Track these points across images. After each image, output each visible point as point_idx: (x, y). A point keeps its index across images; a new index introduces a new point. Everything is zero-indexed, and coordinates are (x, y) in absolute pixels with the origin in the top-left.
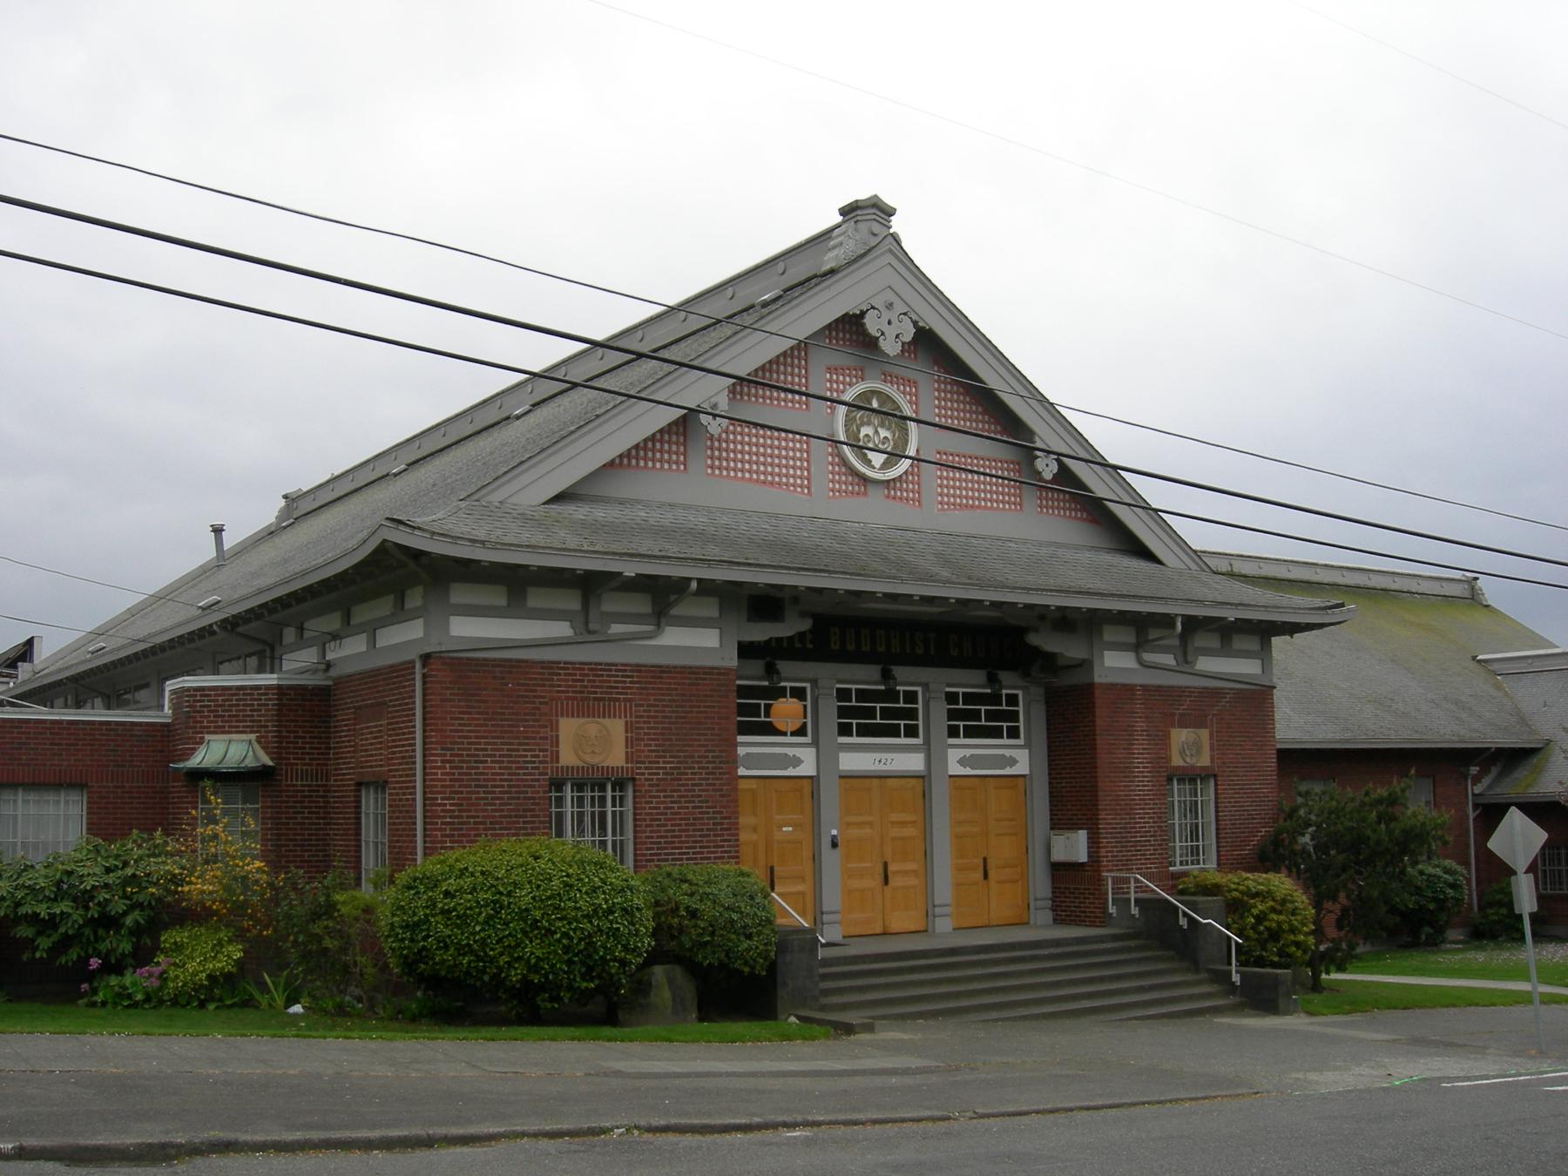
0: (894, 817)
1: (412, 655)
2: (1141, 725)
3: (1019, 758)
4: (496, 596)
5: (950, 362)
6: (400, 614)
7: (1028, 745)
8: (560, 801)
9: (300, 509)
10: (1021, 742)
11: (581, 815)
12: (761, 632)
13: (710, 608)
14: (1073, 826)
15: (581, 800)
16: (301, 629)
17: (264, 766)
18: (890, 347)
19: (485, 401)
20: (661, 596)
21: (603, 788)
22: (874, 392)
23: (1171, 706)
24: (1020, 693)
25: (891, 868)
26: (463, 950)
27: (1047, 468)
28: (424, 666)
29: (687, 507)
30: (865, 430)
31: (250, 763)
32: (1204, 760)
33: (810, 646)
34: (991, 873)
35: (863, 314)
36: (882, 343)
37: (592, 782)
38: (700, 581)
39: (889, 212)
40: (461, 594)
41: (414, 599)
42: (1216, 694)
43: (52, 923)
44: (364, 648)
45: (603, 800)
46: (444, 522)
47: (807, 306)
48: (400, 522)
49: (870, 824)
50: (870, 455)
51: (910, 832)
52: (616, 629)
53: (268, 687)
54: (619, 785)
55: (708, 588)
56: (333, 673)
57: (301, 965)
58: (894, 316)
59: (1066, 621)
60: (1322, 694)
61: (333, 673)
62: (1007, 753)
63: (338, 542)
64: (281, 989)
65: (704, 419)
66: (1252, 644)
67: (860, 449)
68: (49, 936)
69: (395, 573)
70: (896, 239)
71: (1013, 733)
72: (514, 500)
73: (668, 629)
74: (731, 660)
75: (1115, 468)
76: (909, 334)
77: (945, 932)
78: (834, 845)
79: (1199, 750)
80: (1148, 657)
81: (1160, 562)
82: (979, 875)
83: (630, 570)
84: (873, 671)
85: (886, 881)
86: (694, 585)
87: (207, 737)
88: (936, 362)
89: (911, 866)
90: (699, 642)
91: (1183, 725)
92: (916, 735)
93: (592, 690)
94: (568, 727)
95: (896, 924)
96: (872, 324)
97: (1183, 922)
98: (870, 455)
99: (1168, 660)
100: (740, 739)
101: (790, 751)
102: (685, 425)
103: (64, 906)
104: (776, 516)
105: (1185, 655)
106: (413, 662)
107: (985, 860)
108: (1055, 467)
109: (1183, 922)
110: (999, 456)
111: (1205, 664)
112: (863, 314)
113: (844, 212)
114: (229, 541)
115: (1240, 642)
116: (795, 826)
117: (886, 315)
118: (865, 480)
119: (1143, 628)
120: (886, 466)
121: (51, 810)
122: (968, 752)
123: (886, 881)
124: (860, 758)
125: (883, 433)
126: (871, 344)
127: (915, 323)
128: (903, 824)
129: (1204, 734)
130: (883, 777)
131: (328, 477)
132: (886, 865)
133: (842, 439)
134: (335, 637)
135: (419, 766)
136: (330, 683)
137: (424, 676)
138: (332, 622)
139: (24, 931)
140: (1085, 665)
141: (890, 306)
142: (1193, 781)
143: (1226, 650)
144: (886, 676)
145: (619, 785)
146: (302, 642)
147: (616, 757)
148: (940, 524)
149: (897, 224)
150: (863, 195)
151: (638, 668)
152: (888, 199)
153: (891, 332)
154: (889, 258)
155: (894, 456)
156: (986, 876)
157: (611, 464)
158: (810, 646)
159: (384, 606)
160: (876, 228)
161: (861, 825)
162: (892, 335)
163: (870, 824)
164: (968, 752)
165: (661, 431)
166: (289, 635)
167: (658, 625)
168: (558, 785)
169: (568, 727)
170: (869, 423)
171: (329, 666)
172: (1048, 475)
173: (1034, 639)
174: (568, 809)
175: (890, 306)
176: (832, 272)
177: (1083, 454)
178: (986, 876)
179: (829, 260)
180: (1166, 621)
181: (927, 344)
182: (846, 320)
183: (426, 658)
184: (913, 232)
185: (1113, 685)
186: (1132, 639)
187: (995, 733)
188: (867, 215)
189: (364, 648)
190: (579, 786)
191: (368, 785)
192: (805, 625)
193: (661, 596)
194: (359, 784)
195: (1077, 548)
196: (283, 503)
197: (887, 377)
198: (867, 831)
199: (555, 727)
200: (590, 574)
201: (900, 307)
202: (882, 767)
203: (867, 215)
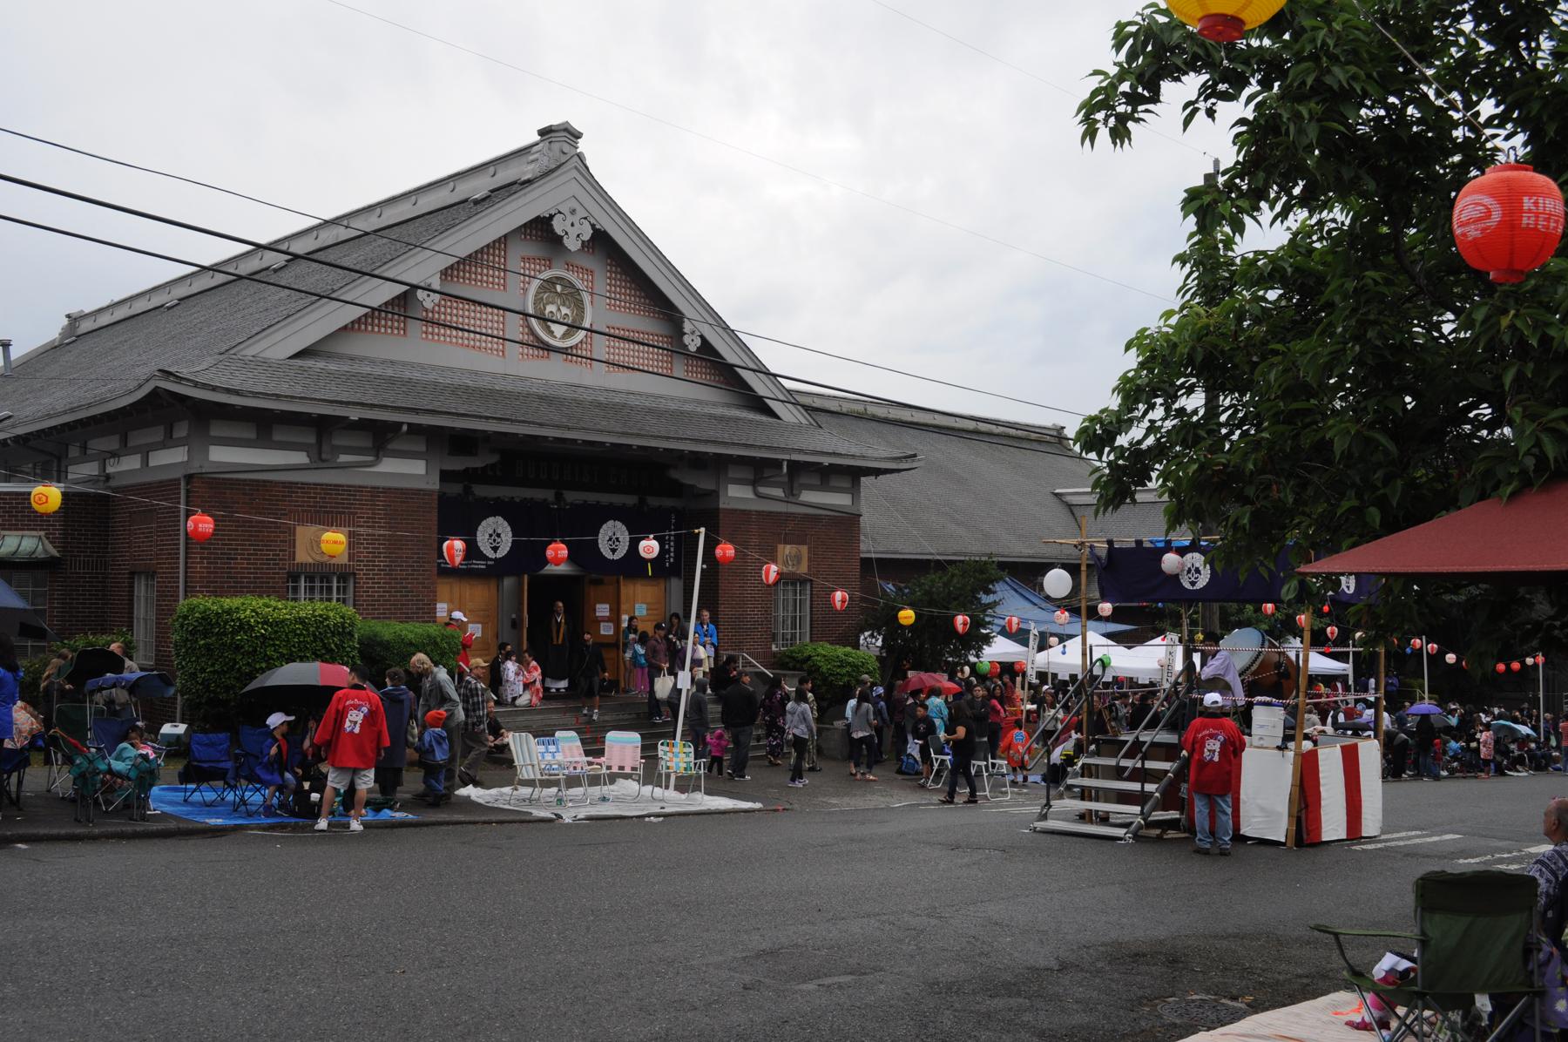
1: (178, 474)
5: (619, 258)
6: (168, 442)
9: (80, 332)
12: (457, 464)
16: (84, 448)
17: (53, 557)
18: (572, 244)
20: (381, 436)
27: (693, 344)
29: (404, 364)
30: (550, 308)
31: (40, 554)
32: (803, 569)
35: (551, 217)
36: (566, 241)
38: (409, 425)
39: (578, 136)
40: (217, 430)
41: (181, 431)
42: (816, 518)
44: (138, 466)
45: (330, 589)
46: (202, 368)
47: (508, 209)
48: (170, 373)
50: (554, 327)
52: (343, 458)
55: (415, 429)
56: (113, 483)
58: (576, 219)
59: (698, 461)
60: (891, 522)
61: (113, 483)
63: (121, 380)
65: (420, 294)
66: (845, 483)
67: (544, 320)
69: (166, 411)
70: (580, 157)
72: (267, 354)
73: (385, 460)
74: (434, 484)
75: (775, 376)
76: (587, 234)
79: (799, 562)
80: (762, 490)
81: (771, 413)
83: (354, 415)
86: (405, 428)
88: (609, 256)
90: (408, 470)
94: (304, 533)
96: (558, 226)
99: (778, 492)
102: (404, 304)
104: (476, 373)
105: (791, 491)
108: (698, 342)
110: (649, 329)
112: (551, 217)
113: (542, 133)
114: (16, 353)
115: (835, 482)
117: (570, 219)
118: (548, 348)
119: (759, 469)
120: (565, 336)
125: (564, 310)
126: (555, 241)
127: (593, 226)
129: (804, 549)
133: (531, 311)
134: (114, 455)
135: (182, 561)
137: (188, 491)
138: (112, 443)
140: (714, 494)
141: (573, 212)
142: (794, 584)
143: (824, 486)
146: (85, 457)
148: (597, 376)
149: (583, 146)
150: (555, 121)
152: (577, 125)
153: (573, 232)
154: (575, 174)
155: (573, 327)
157: (345, 328)
159: (157, 434)
160: (566, 148)
162: (574, 234)
165: (386, 304)
166: (74, 452)
168: (294, 577)
169: (304, 533)
171: (108, 477)
172: (693, 348)
173: (675, 474)
175: (573, 212)
176: (529, 182)
177: (752, 366)
179: (525, 170)
180: (777, 464)
181: (601, 242)
182: (543, 223)
183: (189, 478)
184: (601, 156)
185: (734, 511)
186: (751, 477)
188: (560, 136)
189: (138, 466)
190: (310, 578)
191: (140, 573)
192: (493, 459)
193: (381, 436)
194: (132, 574)
195: (715, 404)
197: (569, 266)
200: (322, 417)
201: (581, 213)
203: (560, 136)
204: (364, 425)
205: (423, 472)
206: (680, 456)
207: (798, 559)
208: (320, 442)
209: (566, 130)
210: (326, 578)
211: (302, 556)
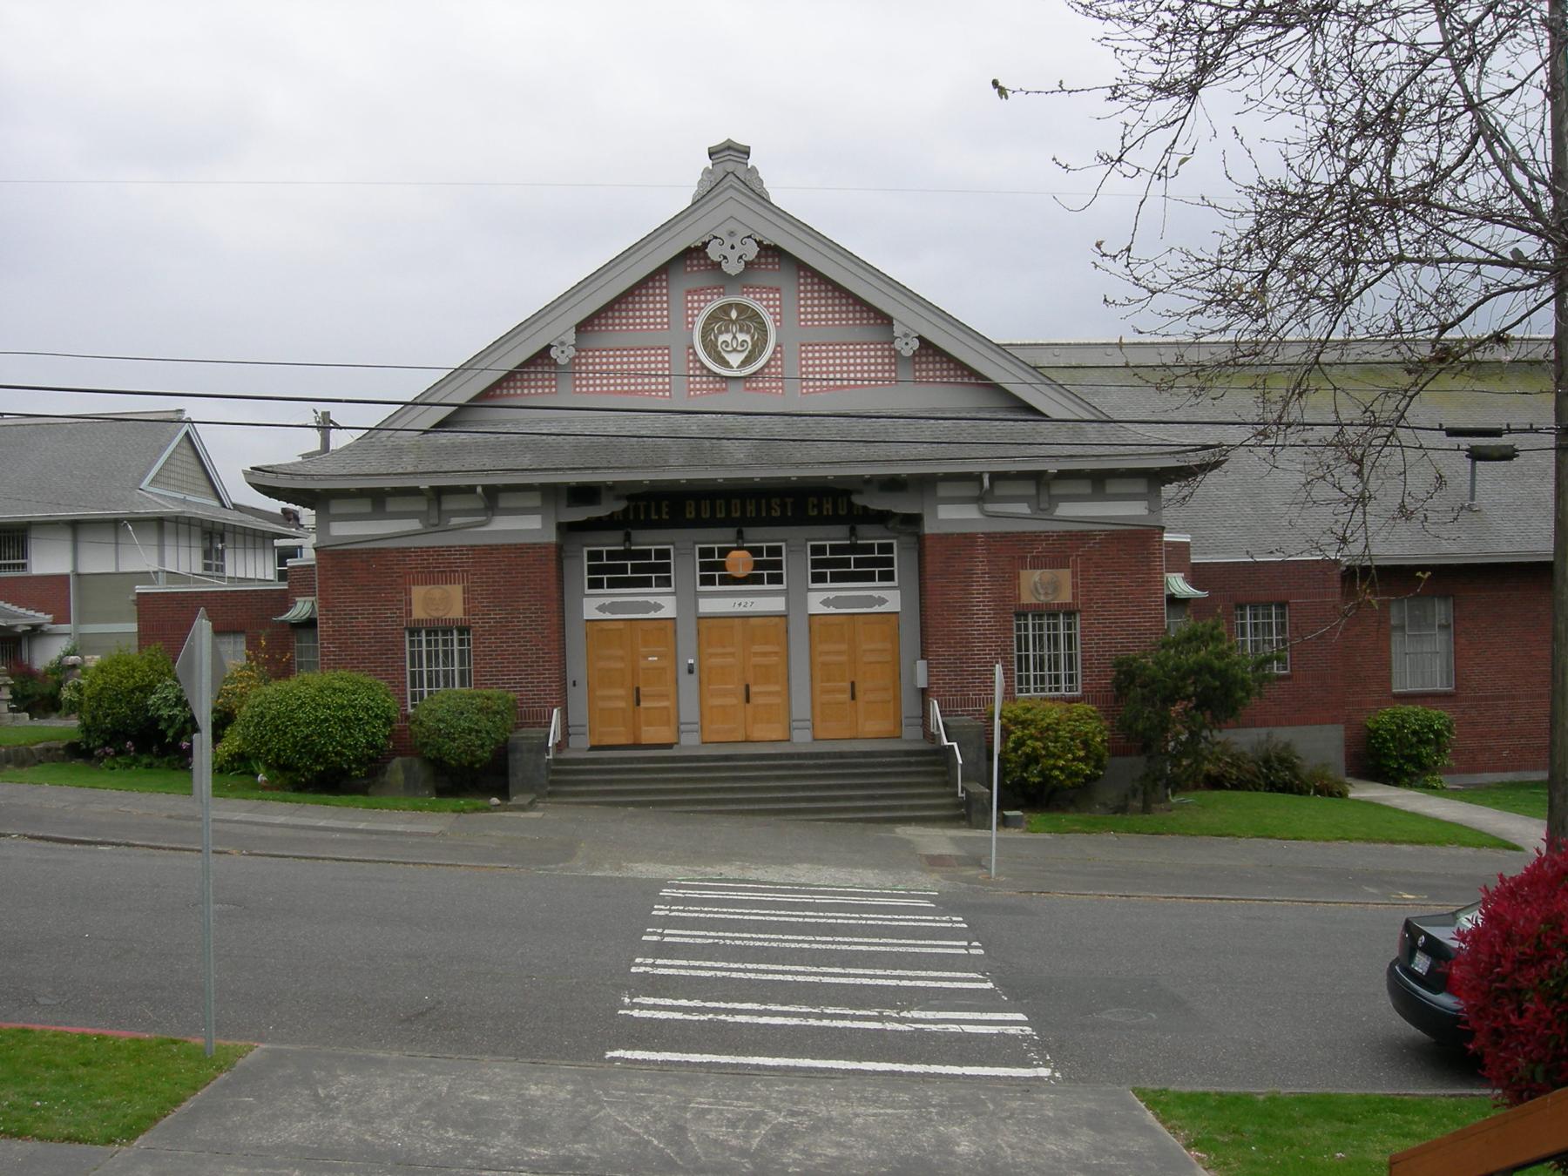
0: (757, 648)
2: (980, 568)
3: (890, 598)
8: (1243, 617)
10: (895, 583)
11: (1041, 636)
13: (535, 500)
18: (733, 267)
20: (493, 498)
21: (1026, 616)
22: (730, 305)
23: (1016, 550)
24: (895, 542)
25: (753, 689)
27: (908, 347)
33: (665, 517)
34: (858, 694)
37: (439, 629)
39: (746, 152)
42: (1083, 536)
49: (732, 654)
51: (844, 658)
52: (455, 521)
54: (1070, 614)
59: (893, 484)
62: (876, 594)
71: (888, 576)
74: (551, 537)
77: (802, 740)
78: (691, 671)
80: (992, 508)
82: (846, 696)
84: (843, 530)
85: (748, 700)
89: (776, 688)
90: (528, 526)
91: (1034, 567)
92: (781, 582)
93: (436, 566)
94: (418, 593)
95: (757, 735)
98: (729, 358)
101: (652, 600)
107: (853, 684)
108: (916, 344)
111: (1066, 510)
112: (705, 245)
116: (660, 656)
122: (832, 595)
123: (748, 700)
124: (717, 603)
125: (741, 337)
127: (759, 243)
128: (765, 654)
130: (746, 617)
132: (747, 687)
141: (732, 234)
144: (853, 532)
145: (1070, 614)
147: (456, 612)
150: (717, 141)
151: (473, 548)
152: (741, 140)
153: (733, 256)
154: (731, 193)
156: (853, 697)
158: (665, 517)
161: (723, 655)
163: (732, 654)
164: (832, 595)
169: (418, 593)
170: (727, 331)
173: (858, 500)
178: (853, 697)
185: (947, 536)
187: (869, 577)
188: (729, 155)
190: (1254, 607)
192: (620, 506)
193: (493, 498)
198: (730, 660)
199: (408, 592)
202: (742, 609)
204: (361, 493)
205: (539, 526)
206: (868, 481)
207: (1056, 587)
208: (1038, 494)
209: (729, 148)
210: (447, 631)
211: (418, 613)
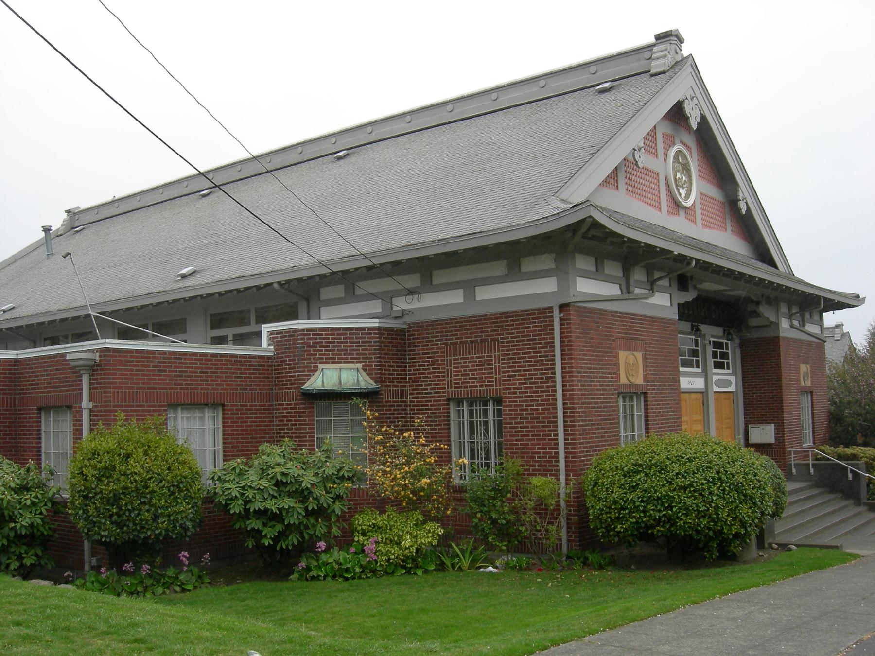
4: (499, 268)
7: (734, 373)
14: (763, 420)
15: (471, 413)
19: (284, 149)
21: (485, 403)
26: (701, 515)
28: (560, 312)
43: (277, 517)
53: (370, 329)
57: (488, 532)
64: (467, 555)
68: (273, 527)
87: (321, 366)
97: (850, 476)
100: (681, 369)
103: (287, 502)
106: (550, 309)
109: (850, 476)
121: (197, 425)
131: (109, 198)
136: (405, 326)
137: (561, 319)
139: (254, 524)
152: (683, 34)
167: (652, 289)
174: (491, 419)
183: (563, 307)
189: (461, 300)
196: (65, 216)
199: (616, 356)
203: (669, 38)
